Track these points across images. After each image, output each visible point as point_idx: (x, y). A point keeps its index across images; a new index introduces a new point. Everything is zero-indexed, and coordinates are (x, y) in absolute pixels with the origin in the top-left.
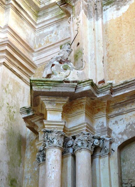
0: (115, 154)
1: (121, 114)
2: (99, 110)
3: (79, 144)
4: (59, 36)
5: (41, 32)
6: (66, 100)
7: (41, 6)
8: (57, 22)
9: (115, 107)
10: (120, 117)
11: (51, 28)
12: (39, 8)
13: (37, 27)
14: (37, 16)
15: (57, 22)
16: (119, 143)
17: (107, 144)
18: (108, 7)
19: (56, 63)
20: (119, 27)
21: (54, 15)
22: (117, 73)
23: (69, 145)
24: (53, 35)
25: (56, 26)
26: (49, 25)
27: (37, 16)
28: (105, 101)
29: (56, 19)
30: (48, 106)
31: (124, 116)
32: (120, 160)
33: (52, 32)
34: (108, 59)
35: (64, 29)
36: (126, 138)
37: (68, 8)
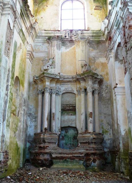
0: (61, 95)
1: (64, 85)
2: (58, 82)
3: (54, 92)
4: (43, 48)
5: (36, 44)
6: (51, 79)
7: (38, 35)
8: (43, 43)
9: (63, 83)
10: (63, 85)
11: (40, 44)
12: (37, 35)
13: (35, 41)
14: (36, 38)
15: (43, 43)
16: (62, 93)
17: (59, 92)
18: (63, 46)
19: (49, 66)
20: (65, 56)
21: (42, 40)
22: (64, 71)
23: (9, 14)
24: (41, 47)
25: (42, 44)
26: (39, 43)
27: (36, 38)
28: (61, 81)
29: (43, 41)
30: (47, 80)
31: (64, 86)
32: (62, 97)
33: (40, 45)
34: (62, 66)
35: (45, 47)
36: (64, 92)
37: (101, 67)
